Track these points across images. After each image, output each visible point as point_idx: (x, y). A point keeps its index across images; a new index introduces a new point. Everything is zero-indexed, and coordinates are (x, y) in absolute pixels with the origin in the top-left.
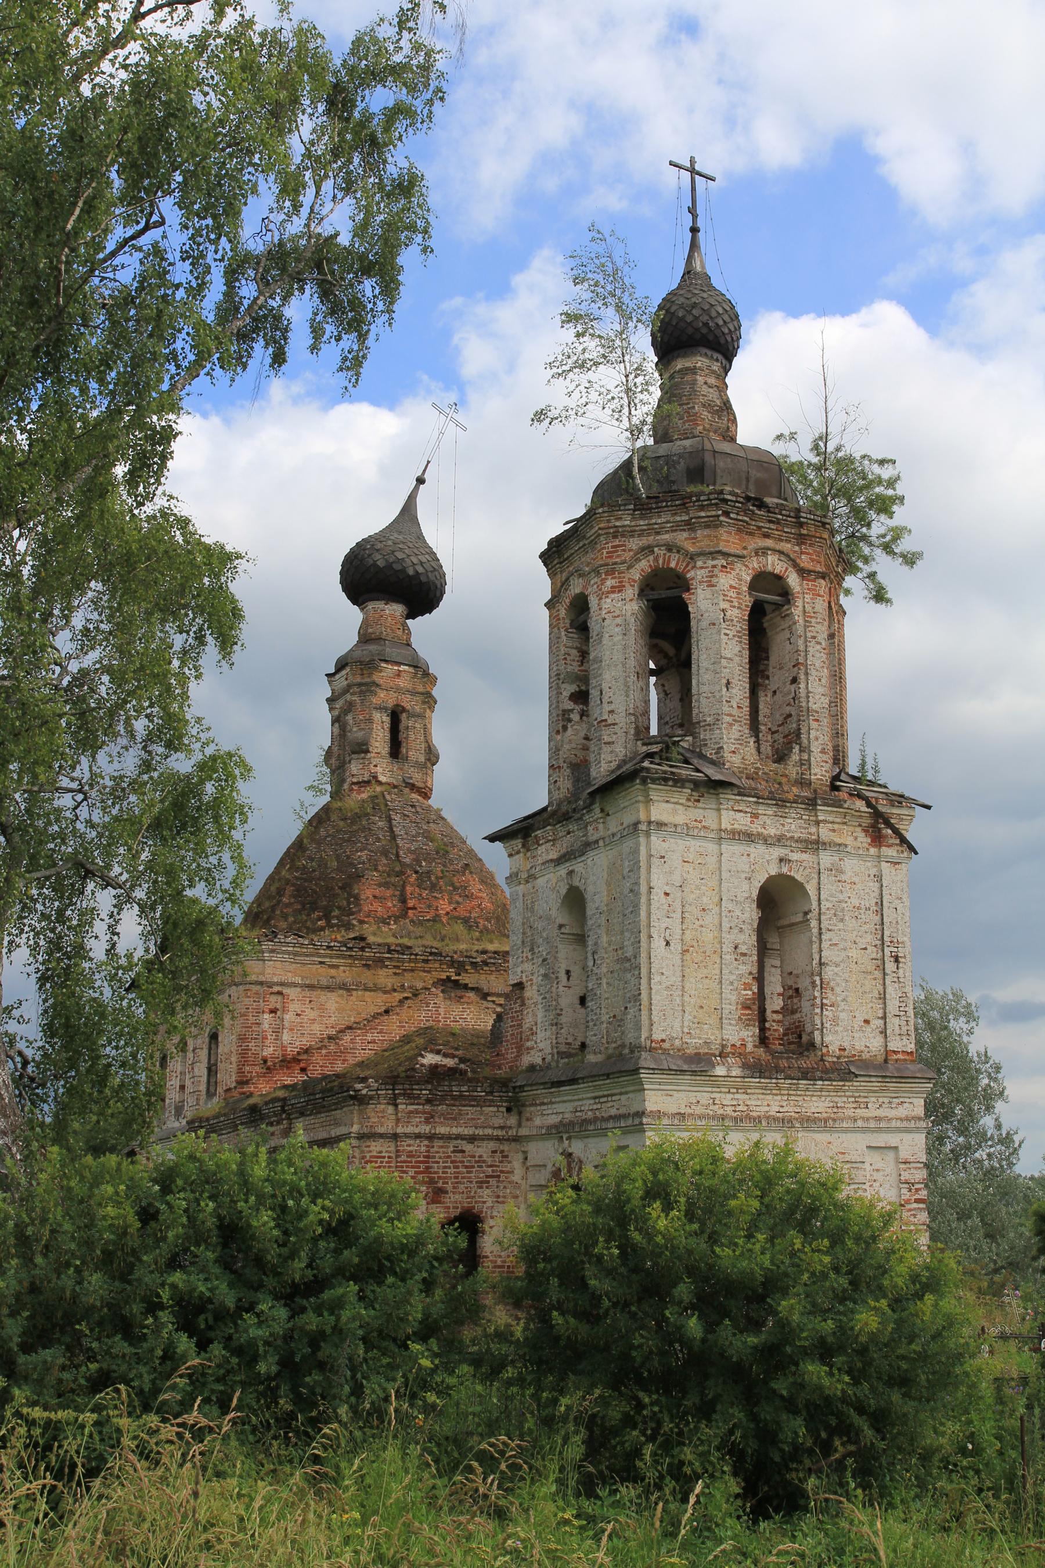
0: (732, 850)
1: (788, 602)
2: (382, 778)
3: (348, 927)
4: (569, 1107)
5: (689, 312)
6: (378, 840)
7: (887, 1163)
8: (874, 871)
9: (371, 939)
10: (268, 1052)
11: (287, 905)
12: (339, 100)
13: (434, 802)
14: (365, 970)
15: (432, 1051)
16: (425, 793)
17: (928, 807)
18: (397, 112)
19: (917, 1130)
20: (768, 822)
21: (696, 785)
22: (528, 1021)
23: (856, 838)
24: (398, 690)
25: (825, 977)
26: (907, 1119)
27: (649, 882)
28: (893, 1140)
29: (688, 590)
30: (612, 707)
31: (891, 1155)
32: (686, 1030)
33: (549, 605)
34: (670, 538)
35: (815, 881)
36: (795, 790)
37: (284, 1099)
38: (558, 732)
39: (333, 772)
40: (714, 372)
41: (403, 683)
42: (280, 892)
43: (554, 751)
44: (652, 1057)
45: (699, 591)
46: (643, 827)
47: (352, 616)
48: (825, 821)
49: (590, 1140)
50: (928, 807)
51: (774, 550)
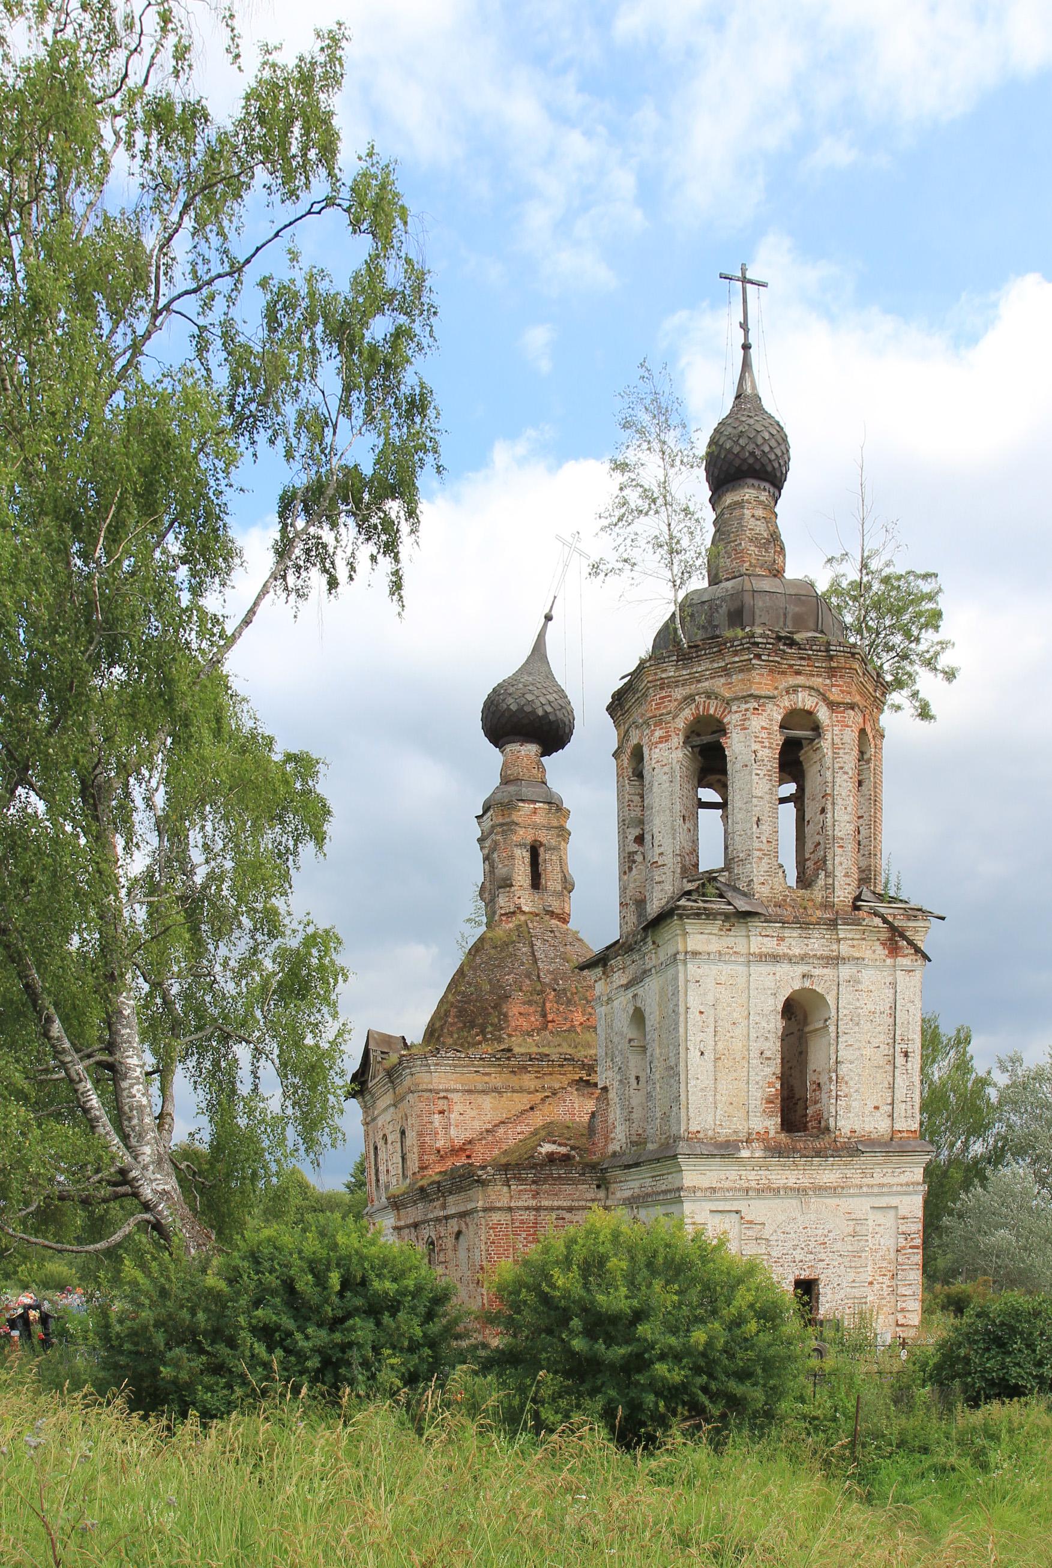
0: (762, 973)
1: (819, 735)
2: (525, 909)
3: (500, 1040)
4: (636, 1184)
5: (736, 442)
6: (523, 964)
7: (888, 1220)
8: (890, 979)
9: (517, 1050)
10: (440, 1144)
11: (452, 1024)
12: (344, 334)
13: (572, 925)
14: (512, 1075)
15: (549, 1142)
16: (564, 919)
17: (943, 919)
18: (400, 334)
19: (916, 1192)
20: (793, 943)
21: (727, 917)
22: (611, 1117)
23: (874, 951)
24: (535, 826)
25: (840, 1073)
26: (907, 1184)
27: (686, 1003)
28: (893, 1201)
29: (725, 734)
30: (662, 850)
31: (892, 1212)
32: (718, 1123)
33: (616, 755)
34: (712, 683)
35: (834, 992)
36: (819, 913)
37: (438, 1182)
38: (625, 873)
39: (486, 905)
40: (761, 503)
41: (538, 819)
42: (447, 1014)
43: (623, 890)
44: (689, 1145)
45: (734, 735)
46: (681, 957)
47: (492, 757)
48: (845, 939)
49: (650, 1209)
50: (943, 919)
51: (804, 687)
